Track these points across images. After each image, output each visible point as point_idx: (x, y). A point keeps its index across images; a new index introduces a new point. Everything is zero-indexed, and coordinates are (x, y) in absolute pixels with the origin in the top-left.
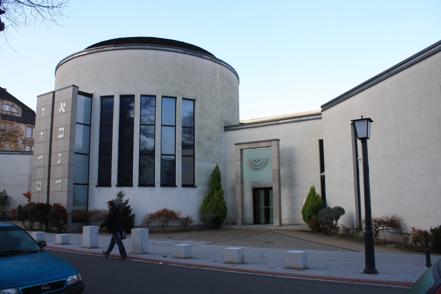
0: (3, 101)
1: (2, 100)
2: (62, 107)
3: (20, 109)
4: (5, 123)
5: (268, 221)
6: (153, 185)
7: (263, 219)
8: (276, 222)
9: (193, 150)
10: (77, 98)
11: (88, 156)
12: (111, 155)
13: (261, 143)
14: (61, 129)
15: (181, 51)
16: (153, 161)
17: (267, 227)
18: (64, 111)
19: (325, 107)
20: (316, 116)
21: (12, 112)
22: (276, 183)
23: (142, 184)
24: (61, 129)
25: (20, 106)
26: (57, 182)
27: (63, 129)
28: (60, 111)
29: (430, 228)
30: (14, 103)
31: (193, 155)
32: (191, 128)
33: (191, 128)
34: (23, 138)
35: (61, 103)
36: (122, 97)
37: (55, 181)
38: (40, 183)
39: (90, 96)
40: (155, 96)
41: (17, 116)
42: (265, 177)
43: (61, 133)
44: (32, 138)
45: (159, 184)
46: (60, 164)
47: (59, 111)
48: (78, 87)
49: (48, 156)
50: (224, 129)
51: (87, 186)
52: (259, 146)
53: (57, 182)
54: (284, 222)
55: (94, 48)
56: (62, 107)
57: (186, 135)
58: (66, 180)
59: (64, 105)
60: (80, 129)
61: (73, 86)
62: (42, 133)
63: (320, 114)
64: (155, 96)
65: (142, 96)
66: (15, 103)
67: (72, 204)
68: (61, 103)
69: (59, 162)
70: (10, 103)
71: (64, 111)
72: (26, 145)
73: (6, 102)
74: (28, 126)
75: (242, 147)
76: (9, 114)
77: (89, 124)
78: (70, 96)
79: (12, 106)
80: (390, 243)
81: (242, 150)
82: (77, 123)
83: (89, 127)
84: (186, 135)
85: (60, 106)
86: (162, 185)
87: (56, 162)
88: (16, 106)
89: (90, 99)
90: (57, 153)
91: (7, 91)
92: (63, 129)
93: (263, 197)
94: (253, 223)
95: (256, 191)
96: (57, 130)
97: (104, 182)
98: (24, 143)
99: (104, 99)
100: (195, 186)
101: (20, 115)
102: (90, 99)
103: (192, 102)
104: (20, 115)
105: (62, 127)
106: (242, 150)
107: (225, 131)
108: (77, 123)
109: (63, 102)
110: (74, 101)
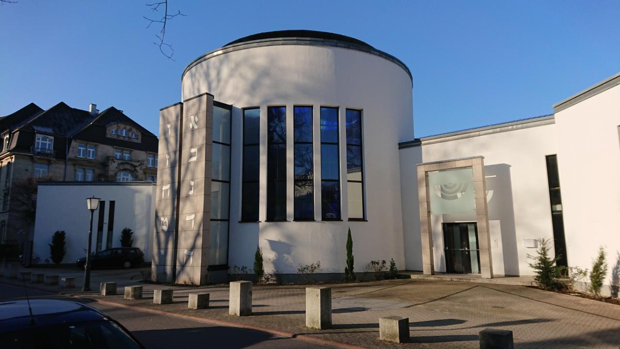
0: (119, 125)
1: (118, 123)
3: (140, 134)
4: (122, 150)
6: (312, 219)
10: (212, 109)
15: (343, 45)
21: (130, 138)
25: (140, 131)
34: (144, 167)
41: (136, 142)
42: (463, 208)
44: (154, 167)
45: (320, 219)
53: (188, 218)
55: (231, 45)
57: (272, 279)
60: (218, 149)
70: (128, 127)
72: (147, 175)
74: (149, 154)
76: (126, 139)
77: (229, 143)
82: (214, 142)
83: (229, 147)
84: (272, 279)
86: (325, 218)
88: (134, 130)
91: (124, 113)
93: (458, 238)
94: (445, 271)
95: (448, 228)
98: (145, 173)
101: (139, 141)
104: (139, 141)
110: (209, 112)
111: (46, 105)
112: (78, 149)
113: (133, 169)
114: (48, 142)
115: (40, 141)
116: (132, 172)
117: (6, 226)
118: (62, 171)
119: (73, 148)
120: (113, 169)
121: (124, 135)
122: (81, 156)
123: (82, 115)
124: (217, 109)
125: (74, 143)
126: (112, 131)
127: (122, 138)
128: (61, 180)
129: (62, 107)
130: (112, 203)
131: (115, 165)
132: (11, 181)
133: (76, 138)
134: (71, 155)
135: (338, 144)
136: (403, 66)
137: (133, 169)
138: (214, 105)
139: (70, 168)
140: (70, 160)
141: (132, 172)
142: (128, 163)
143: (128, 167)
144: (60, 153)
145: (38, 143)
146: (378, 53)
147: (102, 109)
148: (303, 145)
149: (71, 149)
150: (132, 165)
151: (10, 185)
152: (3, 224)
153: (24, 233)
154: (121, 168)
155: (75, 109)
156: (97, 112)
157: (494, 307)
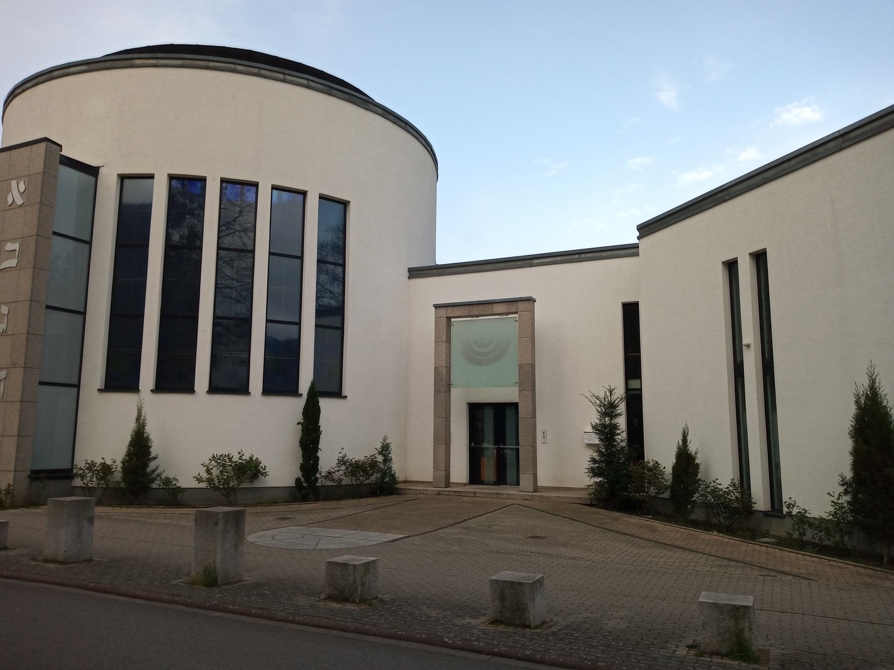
7: (489, 471)
8: (525, 480)
11: (81, 317)
12: (141, 317)
13: (495, 305)
14: (9, 246)
16: (250, 281)
17: (506, 490)
18: (19, 201)
19: (646, 229)
20: (629, 250)
22: (527, 393)
27: (16, 246)
28: (10, 202)
36: (243, 389)
39: (93, 171)
40: (256, 185)
47: (6, 201)
48: (61, 146)
51: (75, 390)
54: (541, 482)
59: (22, 187)
63: (635, 247)
64: (256, 185)
65: (223, 181)
71: (19, 201)
75: (450, 312)
78: (39, 166)
80: (814, 545)
82: (55, 233)
92: (16, 246)
97: (121, 377)
99: (127, 182)
102: (91, 179)
105: (13, 240)
106: (449, 319)
107: (409, 278)
109: (18, 178)
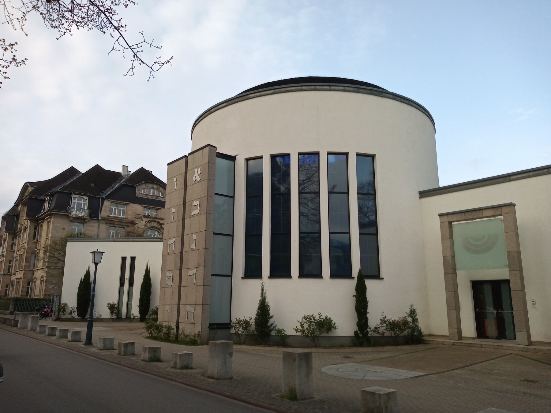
0: (147, 184)
2: (196, 175)
5: (503, 332)
6: (319, 276)
8: (520, 336)
9: (375, 228)
10: (215, 160)
14: (195, 203)
21: (157, 197)
23: (303, 275)
24: (195, 203)
26: (191, 272)
29: (380, 321)
30: (159, 187)
31: (375, 232)
32: (371, 194)
33: (371, 194)
35: (196, 170)
37: (188, 272)
38: (171, 275)
39: (232, 159)
43: (196, 207)
46: (194, 249)
49: (180, 238)
50: (418, 195)
51: (230, 278)
52: (481, 216)
56: (196, 175)
58: (201, 270)
59: (199, 172)
61: (209, 145)
62: (173, 210)
65: (300, 154)
66: (160, 186)
67: (201, 303)
68: (196, 170)
69: (193, 246)
70: (155, 186)
71: (198, 179)
73: (150, 186)
75: (451, 218)
79: (157, 189)
81: (450, 223)
82: (216, 194)
85: (194, 174)
87: (190, 246)
89: (233, 163)
90: (191, 234)
96: (191, 205)
97: (253, 271)
100: (382, 276)
102: (232, 163)
103: (371, 158)
105: (196, 200)
106: (450, 223)
107: (420, 198)
108: (216, 194)
110: (211, 163)
111: (83, 169)
112: (109, 209)
113: (159, 227)
114: (83, 202)
115: (76, 201)
116: (159, 229)
117: (45, 281)
118: (96, 230)
119: (106, 207)
120: (141, 227)
121: (152, 194)
122: (113, 215)
123: (115, 176)
124: (219, 160)
125: (106, 203)
126: (141, 191)
127: (150, 197)
128: (96, 237)
129: (97, 169)
130: (133, 259)
131: (143, 223)
132: (50, 239)
133: (108, 198)
134: (104, 213)
135: (347, 193)
136: (422, 110)
137: (159, 227)
138: (217, 156)
139: (103, 226)
140: (103, 219)
141: (159, 229)
142: (154, 221)
143: (155, 225)
144: (94, 212)
145: (74, 203)
146: (392, 96)
147: (133, 169)
148: (310, 194)
149: (103, 208)
150: (158, 223)
151: (49, 241)
152: (42, 279)
153: (56, 287)
154: (149, 225)
155: (109, 172)
156: (129, 173)
157: (526, 380)
